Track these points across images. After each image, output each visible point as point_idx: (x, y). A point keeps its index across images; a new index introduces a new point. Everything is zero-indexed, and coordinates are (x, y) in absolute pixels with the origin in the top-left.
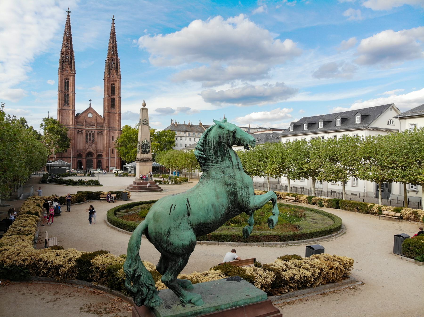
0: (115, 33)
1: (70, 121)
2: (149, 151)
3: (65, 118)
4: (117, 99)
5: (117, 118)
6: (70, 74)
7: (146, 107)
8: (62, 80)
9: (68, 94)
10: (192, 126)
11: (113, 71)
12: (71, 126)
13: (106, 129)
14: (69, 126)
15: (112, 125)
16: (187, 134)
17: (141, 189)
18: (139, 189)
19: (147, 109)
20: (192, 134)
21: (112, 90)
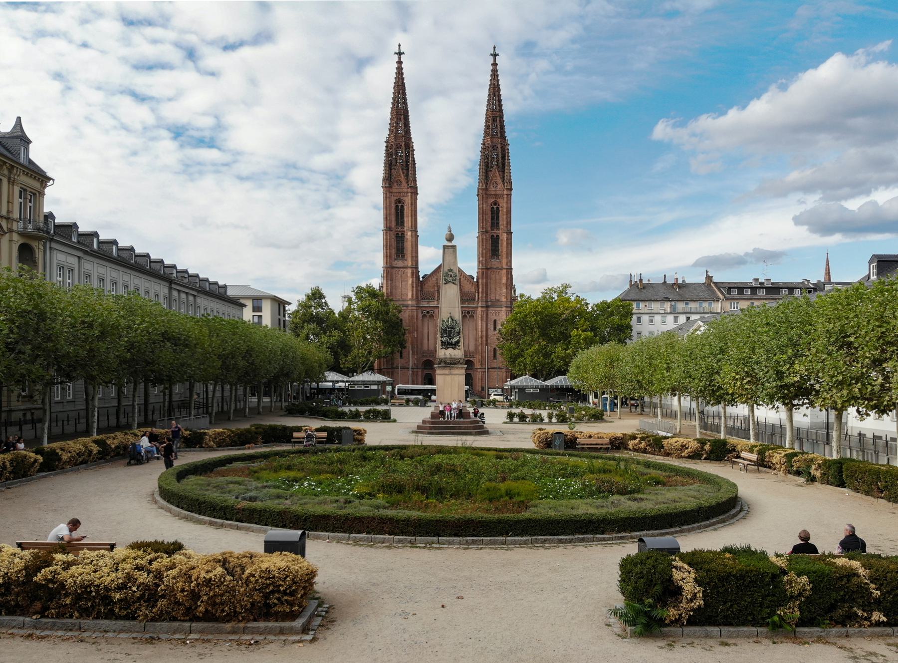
0: (498, 85)
1: (407, 292)
2: (458, 342)
3: (399, 284)
4: (504, 237)
5: (504, 280)
6: (406, 191)
7: (453, 243)
8: (390, 205)
9: (403, 234)
10: (683, 286)
11: (495, 174)
12: (410, 303)
13: (480, 304)
14: (406, 303)
15: (492, 297)
16: (667, 306)
17: (435, 428)
18: (431, 428)
19: (454, 247)
20: (680, 306)
21: (492, 219)
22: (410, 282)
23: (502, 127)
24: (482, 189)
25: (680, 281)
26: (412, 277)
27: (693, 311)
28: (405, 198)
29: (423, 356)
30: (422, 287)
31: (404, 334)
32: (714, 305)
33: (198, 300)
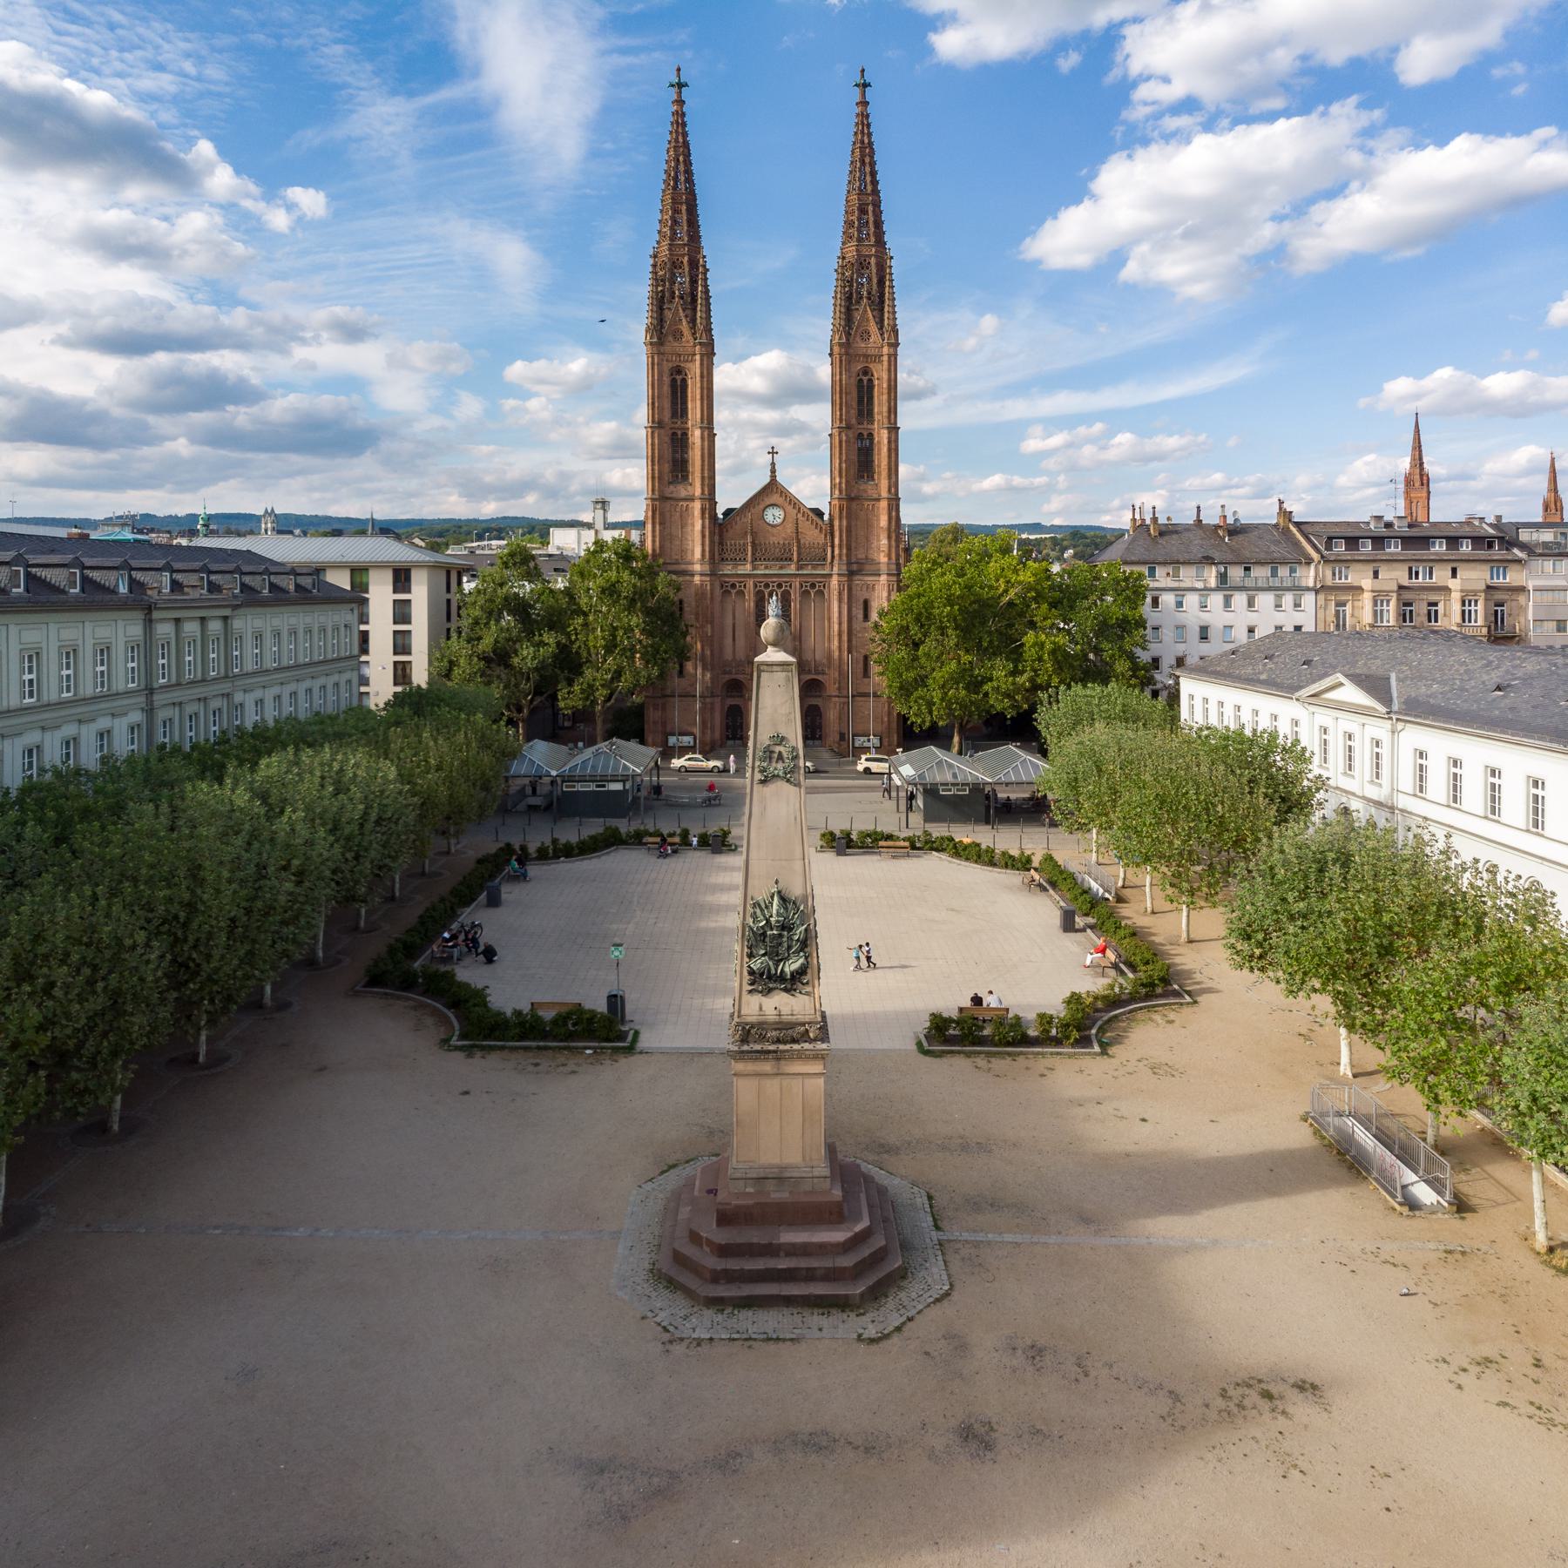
0: (871, 144)
4: (882, 436)
9: (685, 434)
10: (1236, 530)
11: (864, 311)
13: (836, 570)
16: (1211, 575)
21: (860, 401)
22: (698, 526)
25: (1230, 520)
26: (703, 518)
27: (1260, 584)
28: (688, 365)
30: (721, 536)
31: (684, 634)
33: (237, 624)
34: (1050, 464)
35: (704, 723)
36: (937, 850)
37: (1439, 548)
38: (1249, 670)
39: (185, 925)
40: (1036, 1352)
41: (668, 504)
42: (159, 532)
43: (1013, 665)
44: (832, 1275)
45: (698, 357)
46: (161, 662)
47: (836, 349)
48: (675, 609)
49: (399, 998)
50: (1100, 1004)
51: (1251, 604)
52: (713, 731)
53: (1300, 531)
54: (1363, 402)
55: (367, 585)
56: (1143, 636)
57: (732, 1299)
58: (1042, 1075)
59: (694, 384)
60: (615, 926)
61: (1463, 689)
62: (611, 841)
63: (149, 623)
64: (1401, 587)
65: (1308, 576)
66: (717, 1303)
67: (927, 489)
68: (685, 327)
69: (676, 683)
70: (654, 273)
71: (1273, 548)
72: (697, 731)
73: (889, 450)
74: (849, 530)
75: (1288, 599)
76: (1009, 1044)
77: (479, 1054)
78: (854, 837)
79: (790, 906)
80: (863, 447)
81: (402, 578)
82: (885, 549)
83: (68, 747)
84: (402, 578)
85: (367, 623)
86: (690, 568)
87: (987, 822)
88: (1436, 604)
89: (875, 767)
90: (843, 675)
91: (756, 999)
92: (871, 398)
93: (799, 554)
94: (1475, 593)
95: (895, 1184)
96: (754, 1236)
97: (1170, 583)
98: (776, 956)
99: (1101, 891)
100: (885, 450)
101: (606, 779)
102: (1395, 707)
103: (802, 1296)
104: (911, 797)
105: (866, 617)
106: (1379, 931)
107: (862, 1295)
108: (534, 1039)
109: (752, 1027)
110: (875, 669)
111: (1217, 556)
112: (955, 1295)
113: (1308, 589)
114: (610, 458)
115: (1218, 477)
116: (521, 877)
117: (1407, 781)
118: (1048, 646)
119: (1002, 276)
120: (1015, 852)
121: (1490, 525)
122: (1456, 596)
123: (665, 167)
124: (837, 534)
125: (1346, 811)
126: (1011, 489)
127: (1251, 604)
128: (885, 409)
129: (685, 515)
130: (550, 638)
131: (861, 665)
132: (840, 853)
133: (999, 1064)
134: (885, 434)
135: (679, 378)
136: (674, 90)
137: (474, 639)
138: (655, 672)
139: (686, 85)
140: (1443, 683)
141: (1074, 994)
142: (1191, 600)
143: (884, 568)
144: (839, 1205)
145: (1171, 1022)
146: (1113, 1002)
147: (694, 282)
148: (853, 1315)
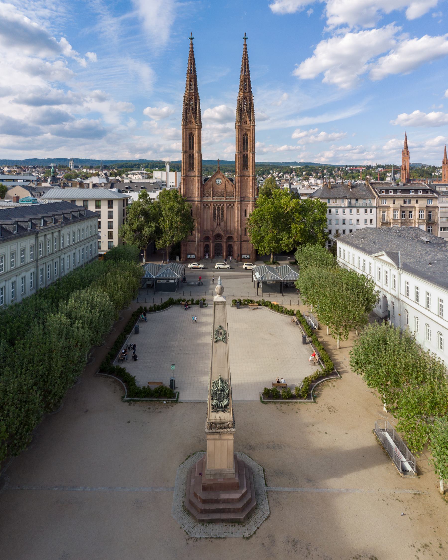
0: (247, 58)
9: (193, 155)
11: (245, 114)
13: (237, 199)
16: (346, 202)
22: (197, 186)
23: (250, 85)
24: (238, 126)
26: (198, 183)
29: (204, 234)
30: (203, 188)
31: (193, 222)
32: (372, 201)
33: (62, 232)
34: (300, 142)
35: (198, 251)
36: (266, 306)
37: (412, 193)
38: (357, 243)
39: (47, 377)
40: (295, 543)
41: (188, 178)
42: (39, 167)
43: (287, 232)
44: (236, 511)
45: (197, 130)
46: (40, 249)
47: (237, 127)
48: (190, 214)
49: (109, 377)
50: (313, 379)
51: (358, 212)
52: (200, 253)
53: (372, 187)
54: (391, 121)
55: (100, 206)
56: (326, 225)
57: (206, 520)
58: (297, 412)
59: (196, 138)
60: (172, 343)
61: (419, 262)
62: (171, 303)
63: (37, 238)
64: (401, 206)
65: (374, 203)
66: (202, 522)
67: (265, 150)
68: (193, 120)
69: (190, 238)
70: (184, 102)
71: (364, 193)
72: (196, 253)
73: (252, 160)
74: (241, 187)
75: (368, 210)
76: (287, 399)
77: (133, 403)
78: (242, 301)
79: (224, 383)
80: (244, 142)
81: (110, 203)
82: (251, 193)
83: (13, 285)
84: (110, 203)
85: (100, 218)
86: (194, 199)
87: (281, 293)
88: (411, 212)
89: (248, 267)
90: (239, 235)
91: (214, 414)
92: (247, 143)
93: (226, 194)
94: (423, 208)
95: (253, 464)
96: (212, 496)
97: (334, 205)
98: (220, 400)
99: (314, 325)
100: (250, 509)
101: (169, 279)
102: (400, 266)
103: (227, 519)
104: (258, 283)
105: (246, 215)
106: (395, 365)
107: (244, 518)
108: (148, 397)
109: (213, 423)
110: (248, 234)
111: (348, 196)
112: (271, 517)
113: (374, 207)
114: (172, 140)
115: (349, 146)
116: (145, 320)
117: (403, 291)
118: (299, 229)
119: (285, 78)
120: (289, 309)
121: (428, 185)
122: (417, 209)
123: (188, 66)
124: (237, 188)
125: (385, 297)
126: (289, 150)
127: (358, 212)
128: (251, 147)
129: (193, 181)
130: (153, 225)
131: (244, 231)
132: (238, 308)
133: (284, 407)
134: (251, 155)
135: (191, 136)
136: (190, 40)
137: (131, 224)
138: (184, 236)
139: (194, 38)
140: (414, 258)
141: (306, 378)
142: (340, 210)
143: (251, 199)
144: (238, 484)
145: (334, 386)
146: (318, 378)
147: (196, 104)
148: (241, 526)
